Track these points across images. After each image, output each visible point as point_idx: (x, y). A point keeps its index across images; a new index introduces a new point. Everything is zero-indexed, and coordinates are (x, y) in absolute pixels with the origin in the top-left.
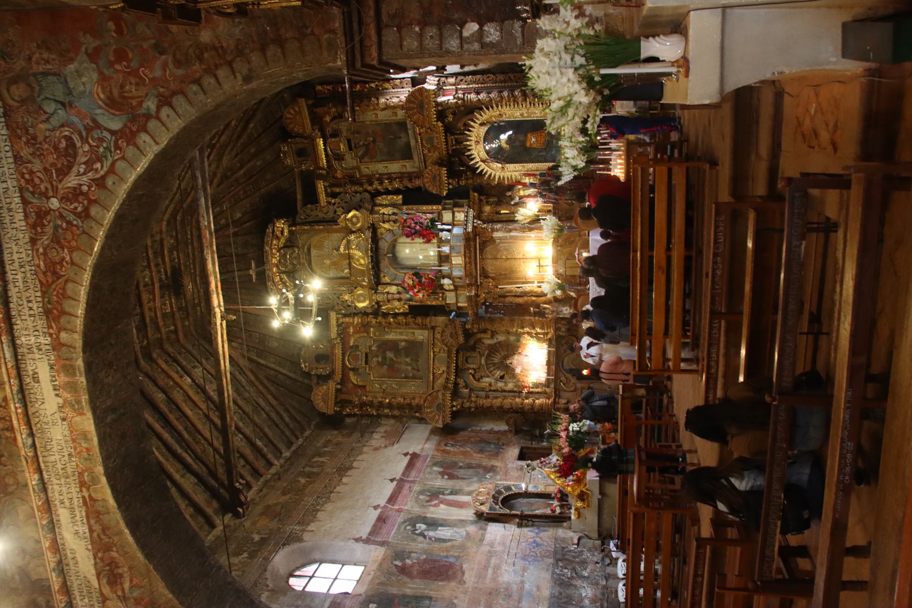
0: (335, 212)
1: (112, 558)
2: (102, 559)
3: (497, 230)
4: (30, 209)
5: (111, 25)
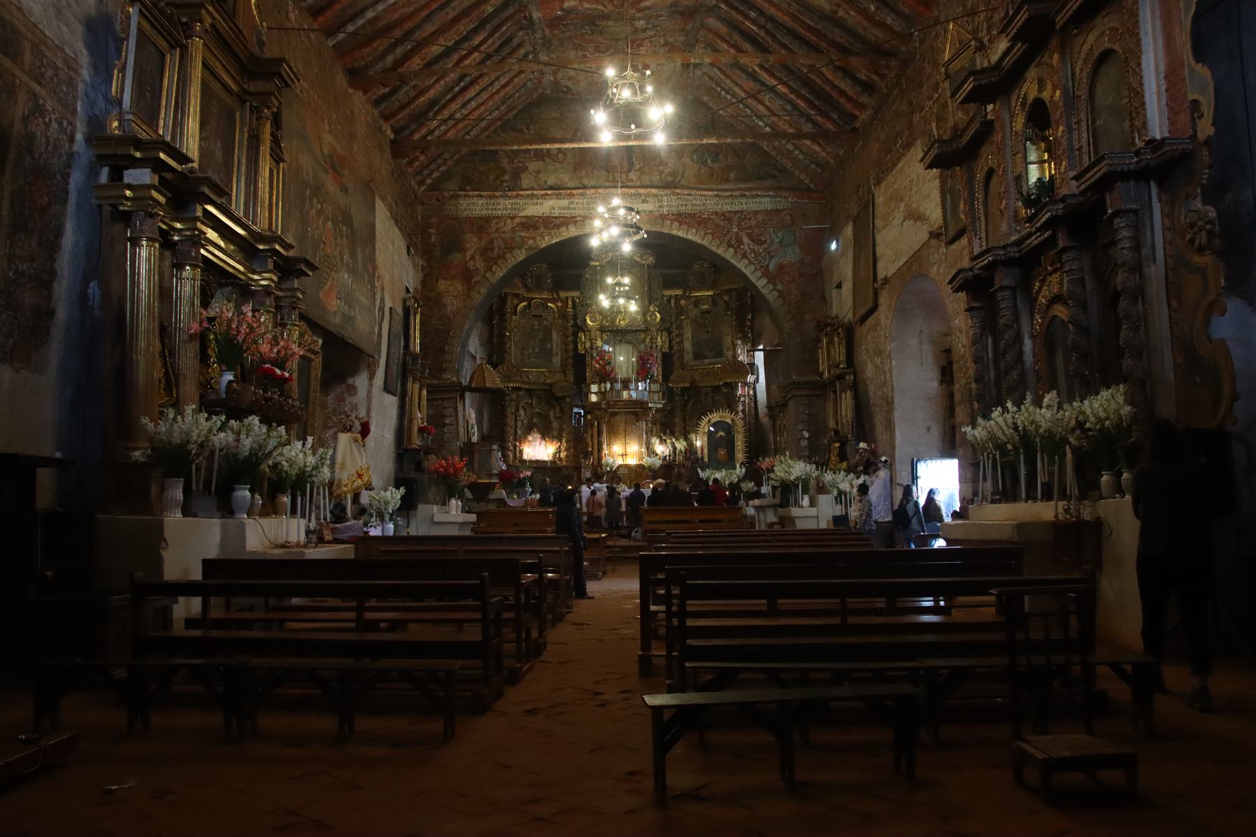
0: (657, 300)
1: (539, 228)
2: (538, 221)
3: (647, 424)
4: (733, 215)
5: (814, 272)
